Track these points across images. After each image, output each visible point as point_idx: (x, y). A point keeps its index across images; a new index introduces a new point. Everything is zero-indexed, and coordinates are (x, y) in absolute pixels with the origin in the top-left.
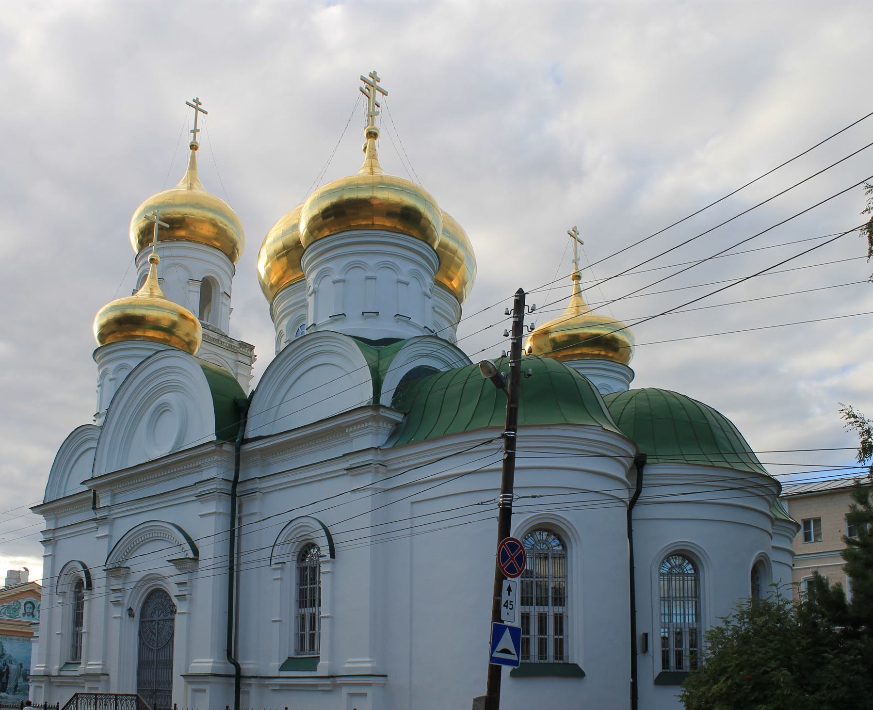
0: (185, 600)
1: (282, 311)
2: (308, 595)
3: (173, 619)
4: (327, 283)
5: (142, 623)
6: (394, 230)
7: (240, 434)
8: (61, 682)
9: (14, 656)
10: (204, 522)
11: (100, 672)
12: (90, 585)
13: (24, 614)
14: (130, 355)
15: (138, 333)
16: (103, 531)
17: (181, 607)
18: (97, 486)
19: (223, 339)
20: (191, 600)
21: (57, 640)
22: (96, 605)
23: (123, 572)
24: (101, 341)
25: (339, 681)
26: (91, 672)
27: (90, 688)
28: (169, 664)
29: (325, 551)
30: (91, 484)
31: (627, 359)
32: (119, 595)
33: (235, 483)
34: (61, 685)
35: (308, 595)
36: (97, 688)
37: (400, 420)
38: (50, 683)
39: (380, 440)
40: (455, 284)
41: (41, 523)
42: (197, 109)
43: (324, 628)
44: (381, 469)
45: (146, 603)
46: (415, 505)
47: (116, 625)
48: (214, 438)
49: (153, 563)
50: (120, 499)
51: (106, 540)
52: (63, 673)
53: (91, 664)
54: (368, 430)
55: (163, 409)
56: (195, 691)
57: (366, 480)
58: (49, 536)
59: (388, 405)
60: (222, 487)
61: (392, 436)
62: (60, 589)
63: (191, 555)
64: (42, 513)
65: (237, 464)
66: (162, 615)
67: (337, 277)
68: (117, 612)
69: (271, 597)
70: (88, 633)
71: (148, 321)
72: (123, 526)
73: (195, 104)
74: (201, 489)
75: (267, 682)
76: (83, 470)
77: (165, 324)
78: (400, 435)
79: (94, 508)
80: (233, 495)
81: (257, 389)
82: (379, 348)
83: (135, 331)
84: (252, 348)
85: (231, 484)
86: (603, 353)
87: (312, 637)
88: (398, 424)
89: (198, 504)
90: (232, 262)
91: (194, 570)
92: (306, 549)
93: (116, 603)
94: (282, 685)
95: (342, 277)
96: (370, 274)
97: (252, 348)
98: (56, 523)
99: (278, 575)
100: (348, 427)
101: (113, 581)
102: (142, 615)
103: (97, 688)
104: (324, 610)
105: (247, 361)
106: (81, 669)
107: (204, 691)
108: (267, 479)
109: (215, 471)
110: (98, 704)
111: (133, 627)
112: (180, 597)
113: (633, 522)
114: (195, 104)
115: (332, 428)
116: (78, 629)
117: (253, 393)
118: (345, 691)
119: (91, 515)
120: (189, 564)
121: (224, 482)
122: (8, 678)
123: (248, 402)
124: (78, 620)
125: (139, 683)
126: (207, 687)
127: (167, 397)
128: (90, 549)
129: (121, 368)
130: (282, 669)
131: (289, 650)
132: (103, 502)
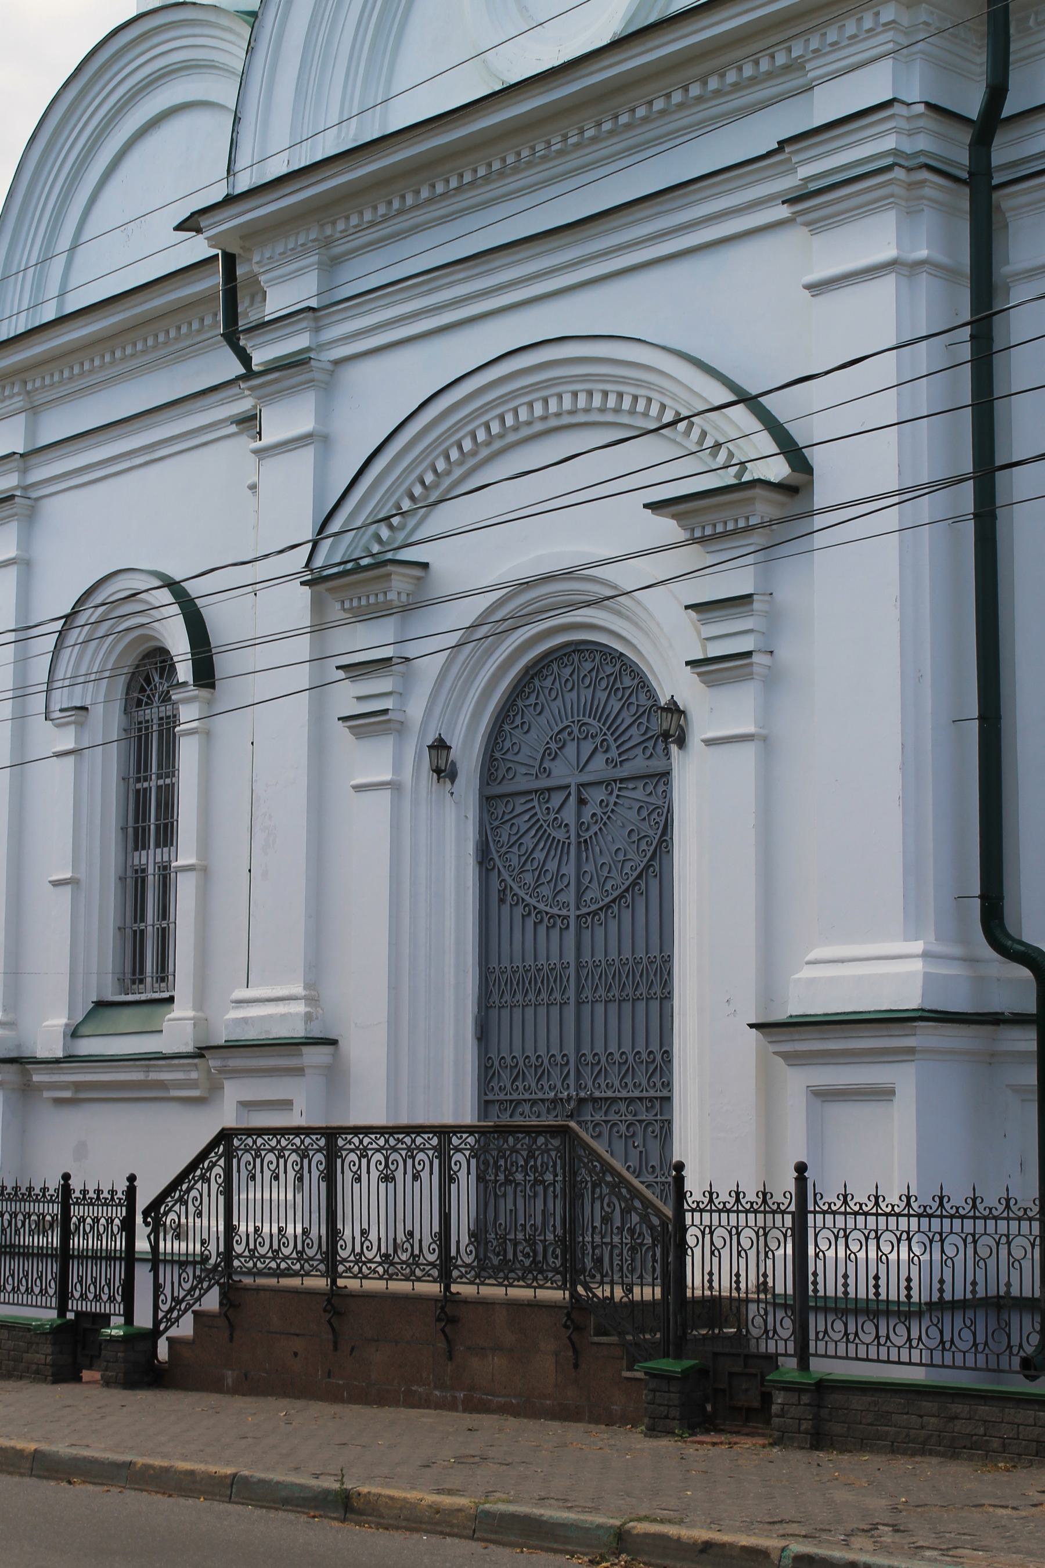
0: (749, 677)
3: (664, 776)
5: (492, 801)
8: (78, 1086)
11: (299, 1031)
12: (205, 673)
17: (714, 713)
20: (772, 681)
23: (399, 584)
26: (251, 1034)
27: (246, 1105)
28: (649, 981)
29: (184, 672)
32: (383, 684)
36: (286, 1105)
38: (27, 1090)
43: (185, 893)
47: (366, 830)
49: (570, 528)
50: (365, 272)
51: (307, 456)
52: (87, 1047)
54: (304, 324)
56: (823, 1095)
60: (922, 143)
62: (61, 699)
63: (777, 470)
66: (599, 761)
68: (374, 762)
70: (203, 870)
72: (383, 393)
74: (810, 167)
85: (966, 136)
89: (797, 235)
93: (367, 724)
98: (31, 431)
103: (286, 1105)
106: (177, 1029)
107: (884, 1094)
111: (453, 827)
116: (150, 858)
120: (763, 508)
121: (930, 122)
124: (148, 815)
125: (488, 1072)
126: (904, 1079)
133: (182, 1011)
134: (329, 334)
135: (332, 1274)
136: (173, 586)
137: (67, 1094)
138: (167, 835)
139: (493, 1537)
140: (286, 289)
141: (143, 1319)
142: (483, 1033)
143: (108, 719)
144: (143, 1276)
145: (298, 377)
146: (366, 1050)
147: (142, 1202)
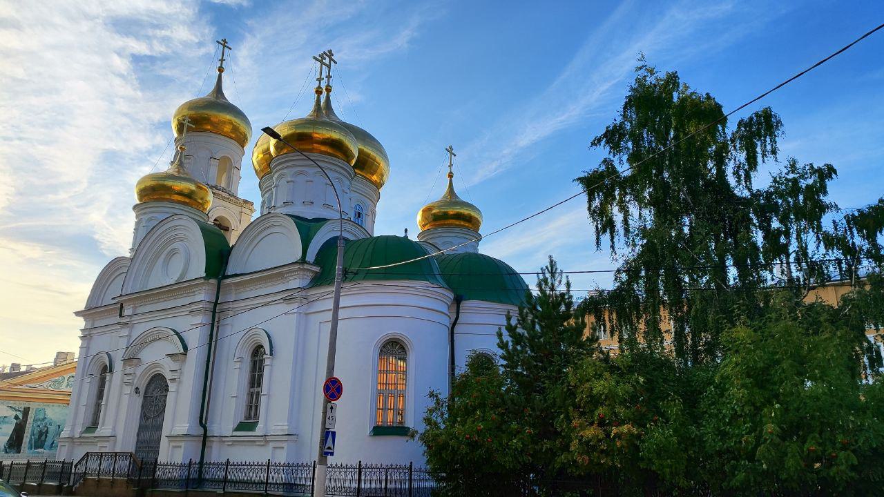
1: (267, 187)
2: (256, 380)
3: (166, 396)
4: (283, 181)
7: (222, 272)
10: (194, 329)
12: (111, 371)
14: (160, 211)
16: (125, 332)
17: (172, 387)
18: (125, 300)
19: (232, 198)
21: (82, 410)
25: (268, 438)
28: (159, 428)
29: (268, 351)
30: (119, 299)
33: (216, 303)
35: (256, 380)
39: (306, 282)
40: (375, 178)
41: (81, 323)
42: (224, 46)
43: (263, 400)
45: (149, 384)
46: (322, 324)
47: (125, 399)
48: (204, 275)
49: (157, 356)
50: (140, 310)
52: (84, 435)
53: (103, 430)
55: (173, 253)
56: (174, 447)
58: (86, 333)
59: (312, 261)
63: (182, 351)
64: (84, 316)
65: (218, 292)
67: (289, 179)
69: (233, 380)
70: (269, 395)
71: (174, 189)
72: (139, 330)
74: (194, 307)
75: (224, 439)
76: (115, 290)
77: (186, 191)
78: (319, 280)
79: (121, 315)
80: (214, 312)
81: (235, 244)
82: (307, 227)
83: (164, 195)
84: (252, 204)
86: (462, 223)
88: (317, 273)
90: (243, 147)
91: (184, 361)
96: (309, 179)
98: (93, 324)
99: (238, 365)
100: (287, 273)
102: (145, 393)
105: (249, 212)
108: (238, 302)
109: (203, 295)
110: (102, 459)
111: (139, 401)
112: (173, 380)
113: (455, 336)
115: (276, 273)
117: (233, 246)
118: (272, 445)
119: (118, 320)
124: (100, 395)
127: (175, 245)
128: (114, 343)
129: (150, 219)
130: (236, 430)
132: (127, 312)
133: (260, 425)
134: (133, 319)
135: (98, 476)
137: (230, 443)
138: (259, 385)
140: (128, 311)
142: (138, 435)
144: (72, 476)
145: (127, 326)
146: (120, 437)
147: (74, 464)
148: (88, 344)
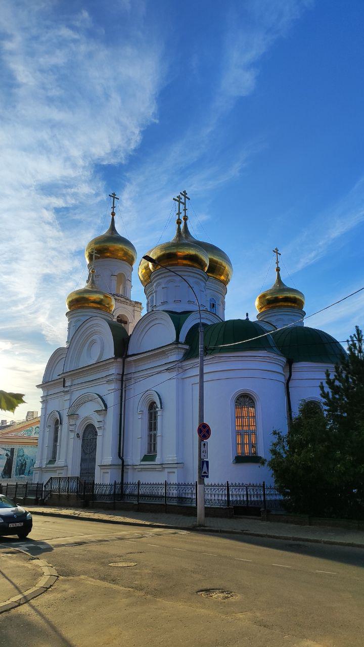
0: (101, 429)
1: (149, 292)
3: (96, 439)
4: (160, 288)
6: (189, 266)
7: (125, 353)
9: (29, 455)
12: (61, 424)
13: (35, 434)
15: (87, 305)
16: (67, 397)
17: (99, 433)
20: (104, 429)
22: (64, 429)
24: (69, 308)
25: (164, 466)
28: (94, 460)
29: (159, 406)
30: (63, 375)
31: (302, 307)
32: (101, 423)
33: (123, 375)
34: (47, 471)
35: (152, 426)
37: (188, 348)
39: (180, 356)
40: (222, 278)
41: (40, 392)
43: (159, 440)
44: (180, 369)
47: (71, 441)
49: (88, 412)
50: (76, 382)
53: (60, 462)
56: (104, 473)
57: (174, 374)
58: (45, 399)
61: (184, 355)
63: (104, 408)
64: (42, 388)
72: (76, 395)
73: (178, 199)
75: (135, 467)
76: (59, 370)
79: (64, 386)
80: (122, 381)
82: (178, 318)
84: (141, 304)
87: (155, 444)
91: (105, 415)
92: (152, 406)
94: (141, 468)
95: (166, 286)
97: (141, 304)
98: (47, 393)
100: (167, 351)
101: (71, 421)
104: (159, 433)
105: (139, 309)
109: (114, 370)
111: (79, 442)
114: (178, 199)
115: (160, 352)
116: (153, 433)
118: (167, 470)
119: (62, 389)
120: (103, 412)
121: (118, 375)
122: (25, 467)
123: (129, 338)
127: (94, 337)
130: (143, 460)
131: (145, 452)
136: (57, 411)
139: (301, 543)
141: (43, 498)
142: (81, 465)
143: (53, 426)
144: (44, 493)
148: (46, 406)
